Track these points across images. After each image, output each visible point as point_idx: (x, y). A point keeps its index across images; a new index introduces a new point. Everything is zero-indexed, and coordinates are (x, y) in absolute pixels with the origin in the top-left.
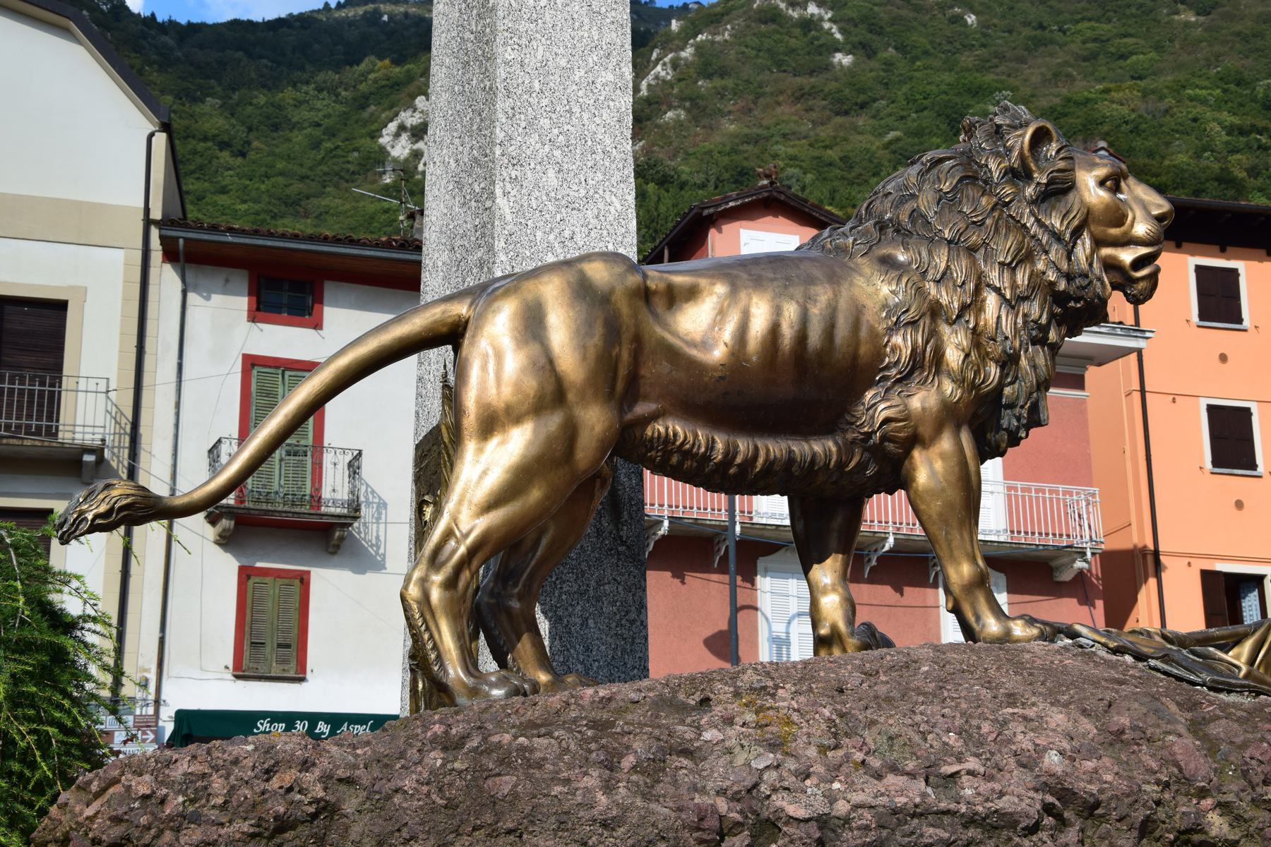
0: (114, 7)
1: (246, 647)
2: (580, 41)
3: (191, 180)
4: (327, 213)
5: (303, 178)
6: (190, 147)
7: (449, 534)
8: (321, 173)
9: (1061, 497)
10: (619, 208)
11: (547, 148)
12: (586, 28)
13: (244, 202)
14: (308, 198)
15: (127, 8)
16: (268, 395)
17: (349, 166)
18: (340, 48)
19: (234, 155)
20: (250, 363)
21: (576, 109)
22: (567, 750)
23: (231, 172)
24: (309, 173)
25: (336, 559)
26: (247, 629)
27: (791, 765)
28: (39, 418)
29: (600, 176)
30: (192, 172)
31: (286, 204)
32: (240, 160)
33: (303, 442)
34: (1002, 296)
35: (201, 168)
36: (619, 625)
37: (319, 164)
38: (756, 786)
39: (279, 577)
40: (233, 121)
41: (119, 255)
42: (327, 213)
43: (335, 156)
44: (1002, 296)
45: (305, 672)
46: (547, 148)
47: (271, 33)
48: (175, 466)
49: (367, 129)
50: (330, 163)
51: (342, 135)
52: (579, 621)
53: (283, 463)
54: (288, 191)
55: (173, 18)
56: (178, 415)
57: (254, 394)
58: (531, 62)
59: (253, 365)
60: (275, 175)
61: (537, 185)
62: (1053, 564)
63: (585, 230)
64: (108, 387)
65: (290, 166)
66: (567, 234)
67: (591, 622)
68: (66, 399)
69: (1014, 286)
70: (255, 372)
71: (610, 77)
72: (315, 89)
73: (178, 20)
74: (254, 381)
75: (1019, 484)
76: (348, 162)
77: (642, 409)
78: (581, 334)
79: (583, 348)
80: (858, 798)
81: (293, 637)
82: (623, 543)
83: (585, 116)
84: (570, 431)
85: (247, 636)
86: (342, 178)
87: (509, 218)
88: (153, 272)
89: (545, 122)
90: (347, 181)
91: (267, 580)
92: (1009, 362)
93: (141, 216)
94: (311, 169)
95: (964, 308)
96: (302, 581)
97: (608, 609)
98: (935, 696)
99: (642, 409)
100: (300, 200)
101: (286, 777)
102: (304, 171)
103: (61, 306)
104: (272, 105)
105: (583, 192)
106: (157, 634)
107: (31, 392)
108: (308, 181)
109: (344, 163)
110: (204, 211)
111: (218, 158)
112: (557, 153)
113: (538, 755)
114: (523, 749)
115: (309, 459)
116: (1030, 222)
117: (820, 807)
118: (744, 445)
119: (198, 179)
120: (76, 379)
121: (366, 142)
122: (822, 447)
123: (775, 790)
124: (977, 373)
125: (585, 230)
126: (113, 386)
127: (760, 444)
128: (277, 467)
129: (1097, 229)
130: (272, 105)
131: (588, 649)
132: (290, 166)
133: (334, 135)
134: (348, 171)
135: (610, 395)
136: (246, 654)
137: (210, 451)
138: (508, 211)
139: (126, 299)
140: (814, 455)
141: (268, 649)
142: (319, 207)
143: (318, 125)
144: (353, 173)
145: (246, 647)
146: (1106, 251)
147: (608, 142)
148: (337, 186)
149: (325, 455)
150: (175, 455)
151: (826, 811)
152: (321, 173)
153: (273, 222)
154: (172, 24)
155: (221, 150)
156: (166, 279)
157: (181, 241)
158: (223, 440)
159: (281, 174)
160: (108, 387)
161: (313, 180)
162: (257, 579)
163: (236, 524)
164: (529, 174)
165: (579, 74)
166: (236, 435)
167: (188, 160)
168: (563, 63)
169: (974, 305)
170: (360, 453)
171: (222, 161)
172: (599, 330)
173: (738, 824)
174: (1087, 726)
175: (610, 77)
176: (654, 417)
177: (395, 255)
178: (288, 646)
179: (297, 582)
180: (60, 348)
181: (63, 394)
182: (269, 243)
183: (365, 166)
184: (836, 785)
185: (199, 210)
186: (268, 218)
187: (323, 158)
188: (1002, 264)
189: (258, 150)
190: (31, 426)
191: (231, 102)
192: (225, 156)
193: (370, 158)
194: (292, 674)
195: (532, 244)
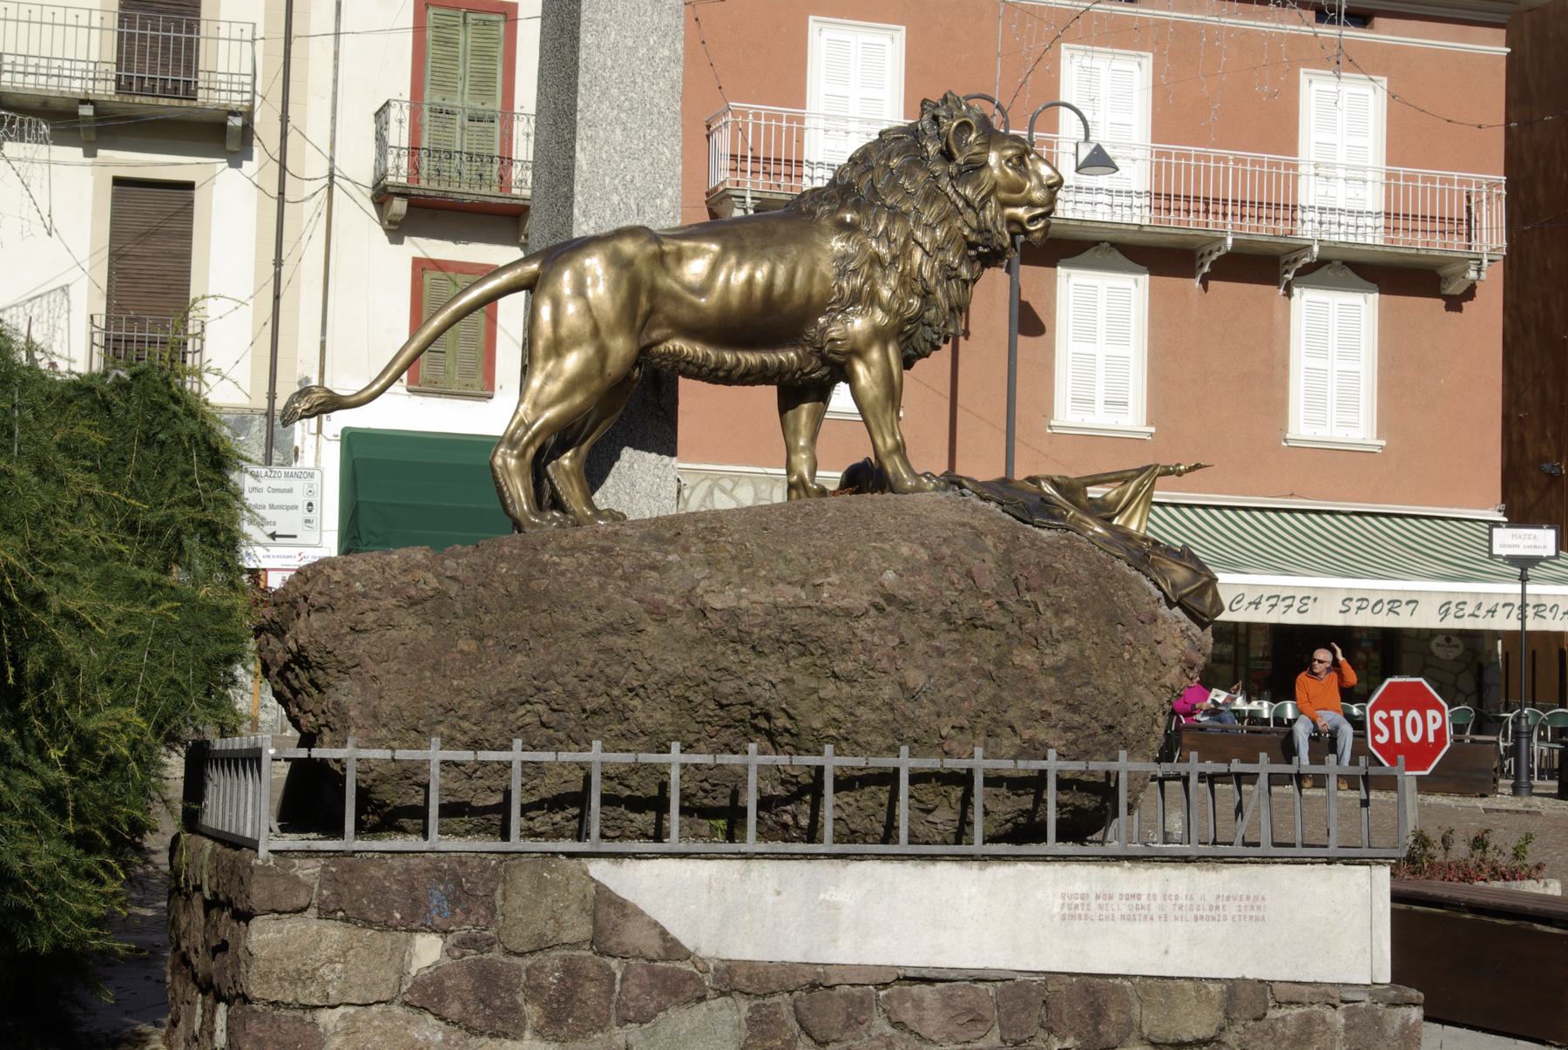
2: (644, 25)
9: (1456, 187)
10: (668, 155)
11: (615, 112)
12: (649, 14)
21: (639, 80)
22: (581, 565)
27: (721, 577)
29: (655, 132)
33: (488, 106)
34: (924, 249)
36: (656, 467)
38: (694, 588)
39: (462, 272)
44: (924, 249)
45: (492, 389)
46: (615, 112)
48: (333, 131)
52: (627, 465)
53: (466, 132)
56: (336, 67)
61: (607, 141)
62: (1442, 272)
63: (642, 175)
64: (254, 33)
66: (628, 178)
67: (636, 466)
68: (205, 48)
69: (934, 240)
70: (431, 11)
71: (667, 53)
75: (1401, 170)
77: (656, 335)
78: (614, 287)
79: (613, 299)
80: (755, 597)
82: (662, 409)
83: (646, 85)
84: (602, 353)
87: (585, 168)
89: (614, 91)
92: (926, 295)
95: (895, 258)
98: (828, 533)
99: (656, 335)
105: (642, 145)
107: (154, 38)
112: (623, 115)
113: (563, 568)
114: (555, 564)
116: (949, 189)
118: (728, 357)
120: (216, 24)
122: (789, 356)
123: (707, 592)
124: (901, 304)
125: (642, 175)
126: (260, 33)
127: (740, 356)
128: (458, 136)
129: (1003, 195)
131: (633, 485)
135: (631, 329)
137: (377, 114)
138: (584, 162)
140: (781, 361)
146: (1009, 211)
147: (662, 104)
149: (515, 123)
150: (334, 118)
151: (735, 604)
158: (393, 103)
160: (254, 33)
163: (409, 206)
164: (601, 133)
166: (407, 97)
168: (630, 44)
169: (904, 254)
172: (624, 286)
173: (679, 611)
175: (667, 53)
176: (666, 339)
181: (202, 42)
184: (744, 590)
188: (926, 225)
194: (477, 391)
195: (603, 186)
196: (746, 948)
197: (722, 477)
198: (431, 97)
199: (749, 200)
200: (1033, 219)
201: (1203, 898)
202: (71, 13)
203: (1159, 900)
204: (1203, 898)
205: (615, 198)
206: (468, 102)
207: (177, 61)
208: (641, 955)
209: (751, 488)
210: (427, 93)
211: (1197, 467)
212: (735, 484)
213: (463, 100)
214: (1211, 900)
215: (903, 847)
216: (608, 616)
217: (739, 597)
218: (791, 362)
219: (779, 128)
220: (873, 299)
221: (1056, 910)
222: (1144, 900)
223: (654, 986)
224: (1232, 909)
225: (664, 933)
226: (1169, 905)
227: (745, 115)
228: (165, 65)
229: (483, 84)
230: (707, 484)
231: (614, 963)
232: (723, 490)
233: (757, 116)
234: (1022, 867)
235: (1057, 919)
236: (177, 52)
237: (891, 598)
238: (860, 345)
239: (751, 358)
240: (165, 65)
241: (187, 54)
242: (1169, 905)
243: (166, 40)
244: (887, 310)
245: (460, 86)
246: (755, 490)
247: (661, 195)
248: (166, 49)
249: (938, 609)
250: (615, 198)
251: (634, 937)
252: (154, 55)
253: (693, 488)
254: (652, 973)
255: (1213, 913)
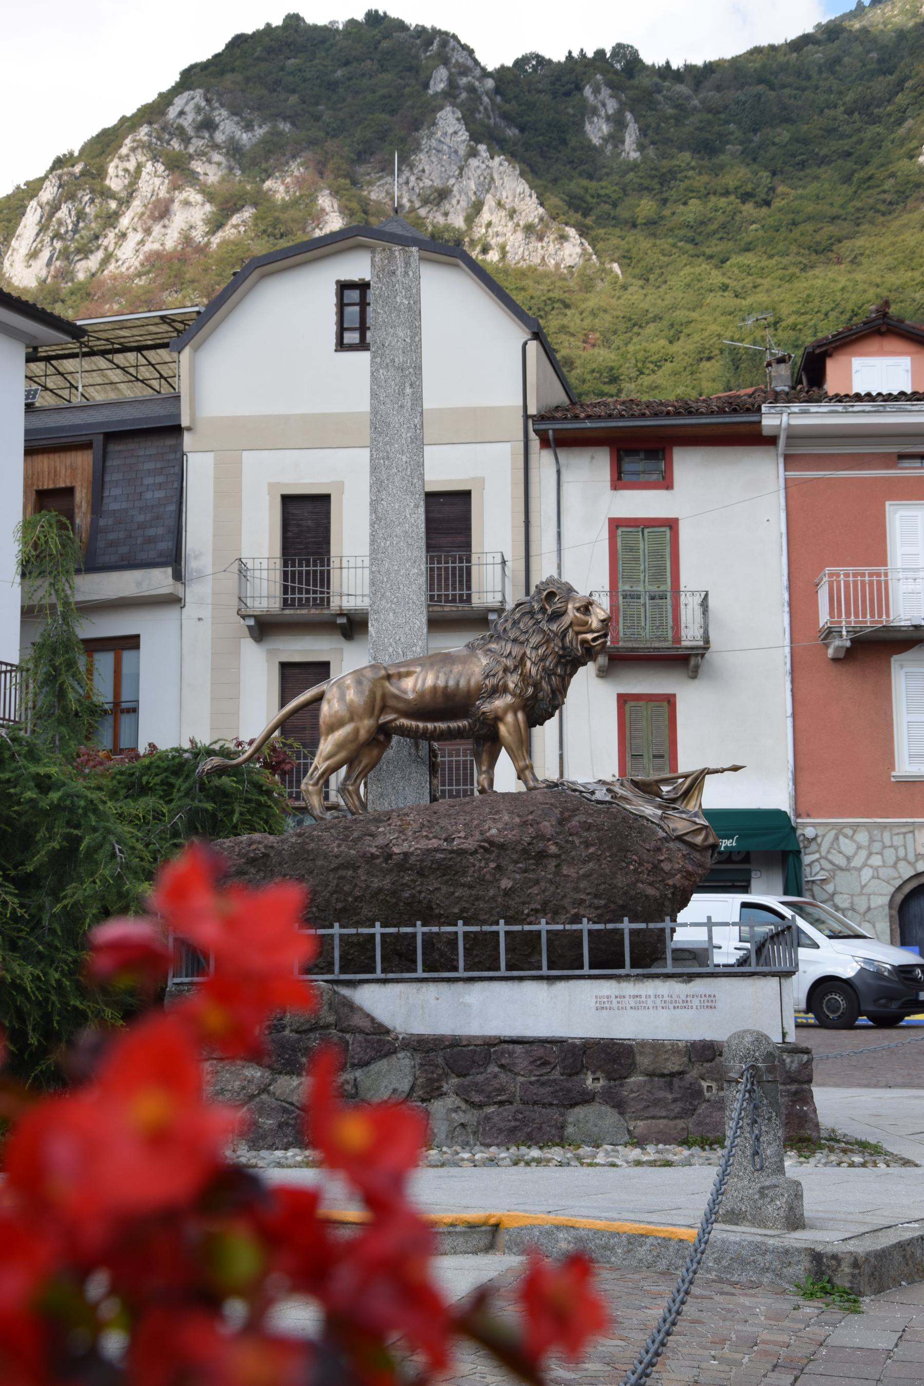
0: (628, 63)
1: (628, 758)
3: (714, 242)
4: (861, 254)
5: (834, 219)
6: (710, 205)
7: (316, 768)
8: (853, 210)
13: (771, 257)
14: (840, 241)
15: (641, 61)
16: (631, 550)
17: (885, 196)
18: (874, 55)
19: (758, 205)
20: (615, 524)
23: (754, 226)
24: (841, 212)
25: (696, 682)
26: (627, 744)
28: (454, 589)
30: (715, 232)
31: (817, 252)
32: (765, 210)
33: (662, 588)
35: (723, 226)
37: (851, 200)
40: (755, 167)
41: (508, 445)
42: (861, 254)
43: (869, 188)
47: (795, 55)
49: (904, 149)
50: (863, 196)
51: (877, 161)
54: (818, 238)
55: (688, 62)
57: (620, 551)
58: (383, 570)
59: (617, 527)
60: (804, 222)
65: (819, 207)
70: (619, 532)
72: (845, 112)
73: (694, 63)
74: (619, 540)
76: (884, 192)
81: (665, 749)
85: (628, 750)
86: (878, 211)
88: (533, 458)
90: (884, 214)
91: (641, 703)
93: (521, 413)
94: (842, 207)
95: (516, 667)
96: (669, 702)
97: (413, 783)
100: (832, 244)
101: (254, 847)
102: (835, 211)
103: (466, 495)
104: (797, 141)
106: (557, 752)
107: (447, 569)
108: (839, 221)
109: (879, 194)
110: (729, 274)
111: (741, 212)
115: (669, 601)
117: (405, 850)
118: (421, 725)
119: (721, 239)
121: (905, 164)
129: (577, 628)
130: (797, 141)
132: (819, 207)
133: (867, 163)
134: (884, 201)
136: (629, 765)
139: (514, 483)
141: (645, 760)
142: (852, 251)
143: (849, 154)
144: (891, 203)
145: (628, 758)
146: (580, 637)
148: (872, 222)
152: (853, 210)
153: (803, 274)
154: (689, 68)
155: (743, 203)
156: (544, 461)
157: (551, 432)
159: (809, 219)
161: (845, 219)
162: (633, 704)
165: (402, 572)
166: (607, 588)
167: (710, 220)
170: (706, 595)
171: (745, 214)
174: (517, 820)
177: (727, 420)
178: (662, 757)
179: (665, 704)
180: (468, 529)
182: (621, 424)
183: (903, 192)
185: (724, 274)
186: (797, 271)
187: (856, 192)
189: (784, 195)
190: (447, 596)
191: (753, 145)
192: (748, 208)
193: (908, 182)
196: (420, 1027)
197: (845, 827)
198: (623, 587)
199: (844, 633)
200: (595, 639)
201: (678, 996)
202: (359, 560)
203: (653, 998)
204: (678, 996)
205: (391, 649)
206: (649, 588)
207: (461, 582)
208: (361, 1032)
209: (866, 834)
210: (620, 585)
211: (735, 769)
212: (855, 832)
213: (644, 587)
214: (683, 997)
215: (503, 972)
216: (340, 860)
217: (410, 846)
218: (464, 726)
219: (863, 582)
220: (505, 690)
221: (593, 1004)
222: (643, 999)
223: (367, 1047)
224: (696, 1002)
225: (373, 1020)
226: (658, 1001)
227: (838, 575)
228: (447, 585)
229: (657, 576)
230: (833, 833)
231: (348, 1036)
232: (846, 836)
233: (847, 575)
234: (572, 983)
235: (594, 1010)
236: (461, 576)
237: (491, 843)
238: (500, 712)
239: (442, 725)
240: (447, 585)
241: (465, 577)
242: (658, 1001)
243: (454, 568)
244: (514, 695)
245: (642, 577)
246: (870, 834)
247: (415, 645)
248: (454, 575)
249: (519, 848)
250: (391, 649)
251: (357, 1021)
252: (447, 579)
253: (824, 836)
254: (367, 1041)
255: (685, 1004)
